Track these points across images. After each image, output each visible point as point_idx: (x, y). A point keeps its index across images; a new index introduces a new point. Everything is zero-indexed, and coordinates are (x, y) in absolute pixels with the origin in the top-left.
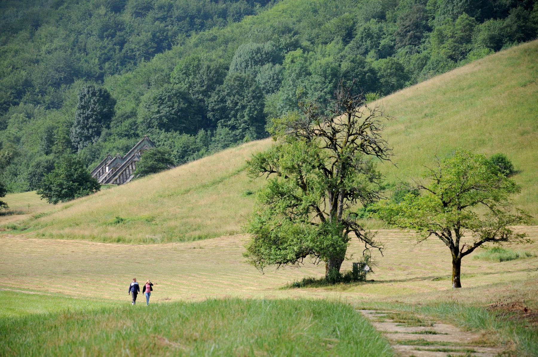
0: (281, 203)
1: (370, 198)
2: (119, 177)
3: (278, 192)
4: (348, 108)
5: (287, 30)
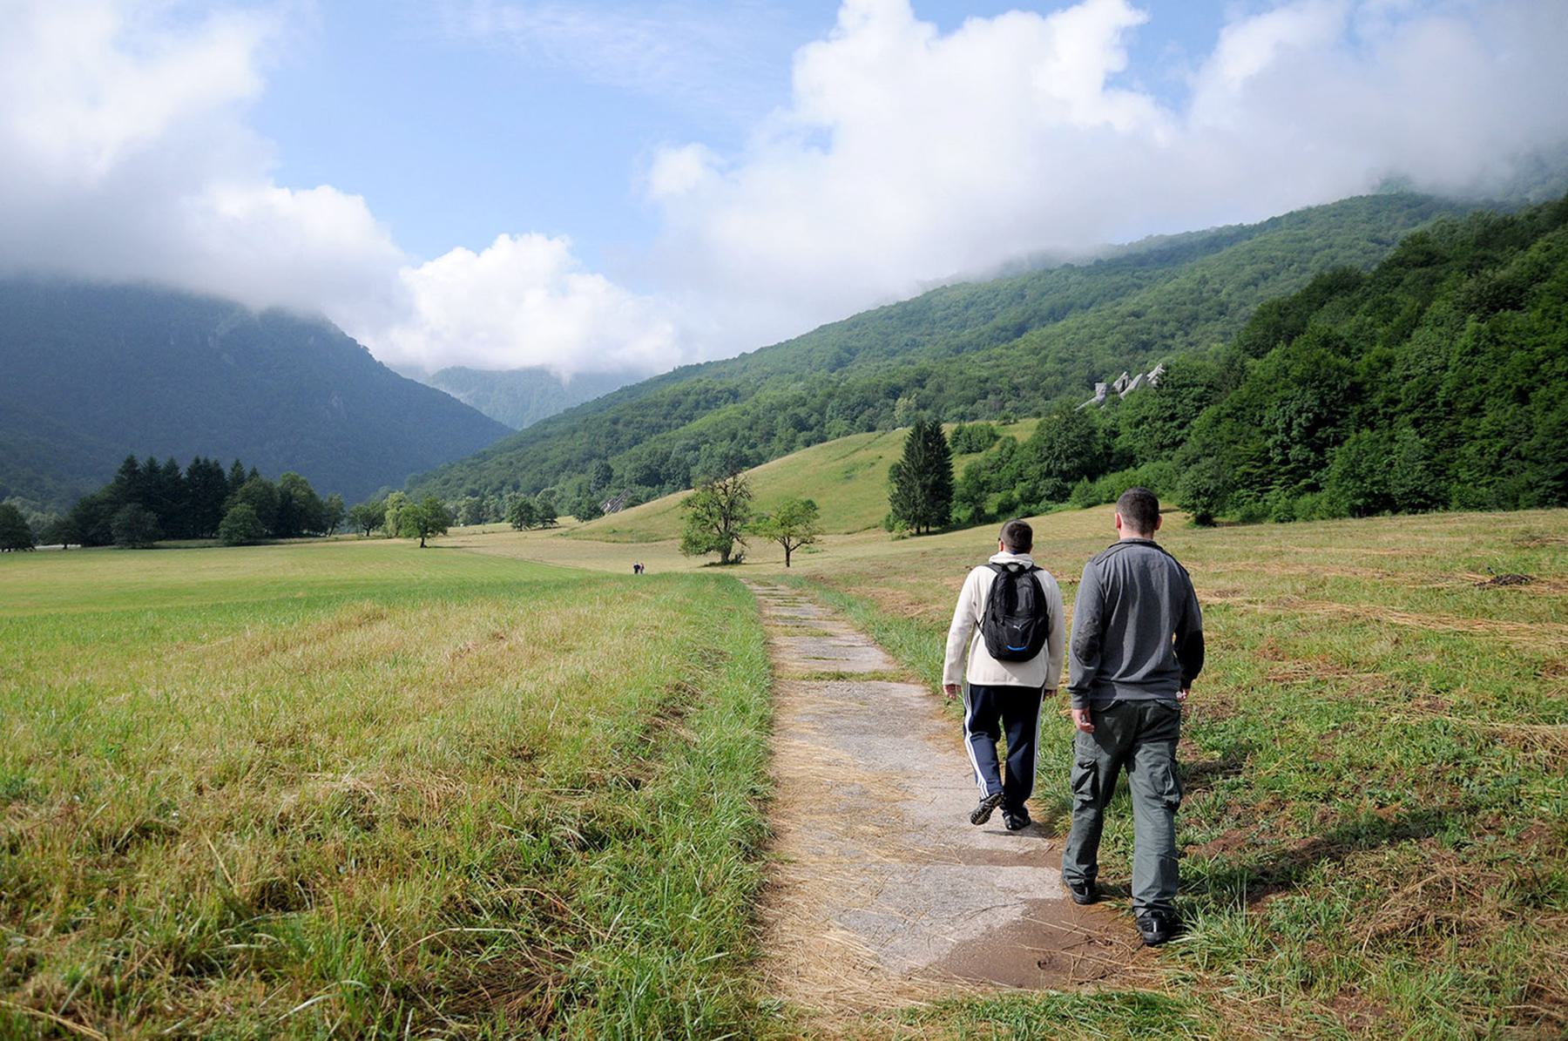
0: (698, 523)
1: (744, 521)
2: (615, 509)
3: (696, 517)
4: (734, 475)
5: (702, 434)
